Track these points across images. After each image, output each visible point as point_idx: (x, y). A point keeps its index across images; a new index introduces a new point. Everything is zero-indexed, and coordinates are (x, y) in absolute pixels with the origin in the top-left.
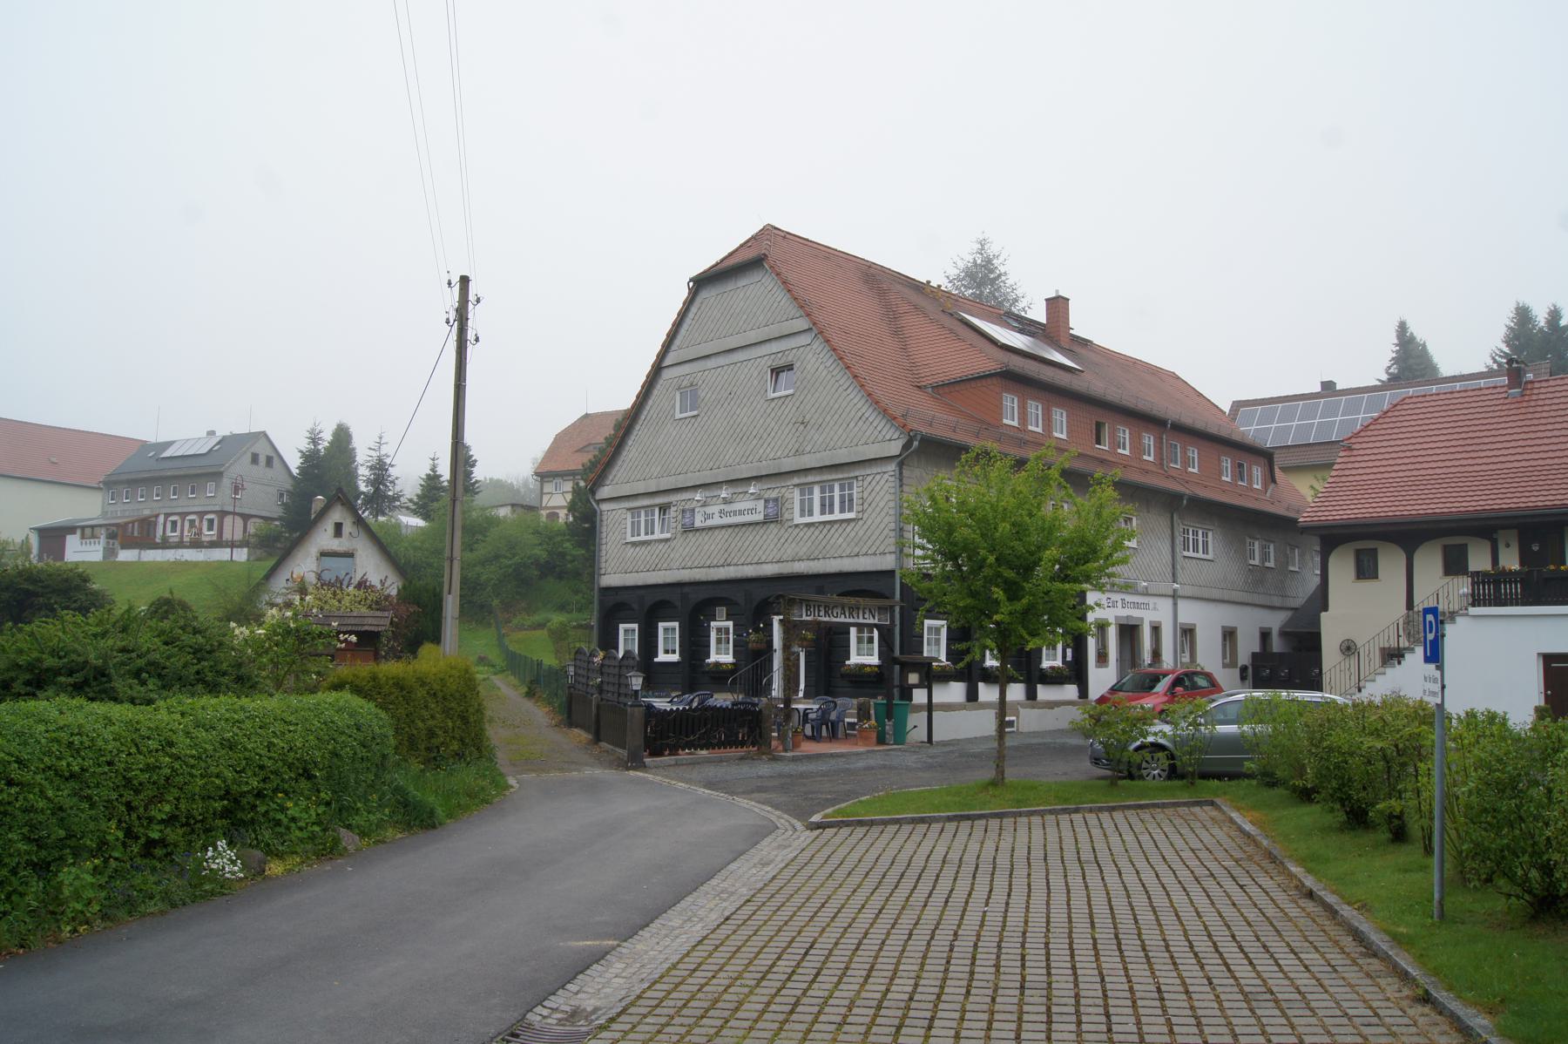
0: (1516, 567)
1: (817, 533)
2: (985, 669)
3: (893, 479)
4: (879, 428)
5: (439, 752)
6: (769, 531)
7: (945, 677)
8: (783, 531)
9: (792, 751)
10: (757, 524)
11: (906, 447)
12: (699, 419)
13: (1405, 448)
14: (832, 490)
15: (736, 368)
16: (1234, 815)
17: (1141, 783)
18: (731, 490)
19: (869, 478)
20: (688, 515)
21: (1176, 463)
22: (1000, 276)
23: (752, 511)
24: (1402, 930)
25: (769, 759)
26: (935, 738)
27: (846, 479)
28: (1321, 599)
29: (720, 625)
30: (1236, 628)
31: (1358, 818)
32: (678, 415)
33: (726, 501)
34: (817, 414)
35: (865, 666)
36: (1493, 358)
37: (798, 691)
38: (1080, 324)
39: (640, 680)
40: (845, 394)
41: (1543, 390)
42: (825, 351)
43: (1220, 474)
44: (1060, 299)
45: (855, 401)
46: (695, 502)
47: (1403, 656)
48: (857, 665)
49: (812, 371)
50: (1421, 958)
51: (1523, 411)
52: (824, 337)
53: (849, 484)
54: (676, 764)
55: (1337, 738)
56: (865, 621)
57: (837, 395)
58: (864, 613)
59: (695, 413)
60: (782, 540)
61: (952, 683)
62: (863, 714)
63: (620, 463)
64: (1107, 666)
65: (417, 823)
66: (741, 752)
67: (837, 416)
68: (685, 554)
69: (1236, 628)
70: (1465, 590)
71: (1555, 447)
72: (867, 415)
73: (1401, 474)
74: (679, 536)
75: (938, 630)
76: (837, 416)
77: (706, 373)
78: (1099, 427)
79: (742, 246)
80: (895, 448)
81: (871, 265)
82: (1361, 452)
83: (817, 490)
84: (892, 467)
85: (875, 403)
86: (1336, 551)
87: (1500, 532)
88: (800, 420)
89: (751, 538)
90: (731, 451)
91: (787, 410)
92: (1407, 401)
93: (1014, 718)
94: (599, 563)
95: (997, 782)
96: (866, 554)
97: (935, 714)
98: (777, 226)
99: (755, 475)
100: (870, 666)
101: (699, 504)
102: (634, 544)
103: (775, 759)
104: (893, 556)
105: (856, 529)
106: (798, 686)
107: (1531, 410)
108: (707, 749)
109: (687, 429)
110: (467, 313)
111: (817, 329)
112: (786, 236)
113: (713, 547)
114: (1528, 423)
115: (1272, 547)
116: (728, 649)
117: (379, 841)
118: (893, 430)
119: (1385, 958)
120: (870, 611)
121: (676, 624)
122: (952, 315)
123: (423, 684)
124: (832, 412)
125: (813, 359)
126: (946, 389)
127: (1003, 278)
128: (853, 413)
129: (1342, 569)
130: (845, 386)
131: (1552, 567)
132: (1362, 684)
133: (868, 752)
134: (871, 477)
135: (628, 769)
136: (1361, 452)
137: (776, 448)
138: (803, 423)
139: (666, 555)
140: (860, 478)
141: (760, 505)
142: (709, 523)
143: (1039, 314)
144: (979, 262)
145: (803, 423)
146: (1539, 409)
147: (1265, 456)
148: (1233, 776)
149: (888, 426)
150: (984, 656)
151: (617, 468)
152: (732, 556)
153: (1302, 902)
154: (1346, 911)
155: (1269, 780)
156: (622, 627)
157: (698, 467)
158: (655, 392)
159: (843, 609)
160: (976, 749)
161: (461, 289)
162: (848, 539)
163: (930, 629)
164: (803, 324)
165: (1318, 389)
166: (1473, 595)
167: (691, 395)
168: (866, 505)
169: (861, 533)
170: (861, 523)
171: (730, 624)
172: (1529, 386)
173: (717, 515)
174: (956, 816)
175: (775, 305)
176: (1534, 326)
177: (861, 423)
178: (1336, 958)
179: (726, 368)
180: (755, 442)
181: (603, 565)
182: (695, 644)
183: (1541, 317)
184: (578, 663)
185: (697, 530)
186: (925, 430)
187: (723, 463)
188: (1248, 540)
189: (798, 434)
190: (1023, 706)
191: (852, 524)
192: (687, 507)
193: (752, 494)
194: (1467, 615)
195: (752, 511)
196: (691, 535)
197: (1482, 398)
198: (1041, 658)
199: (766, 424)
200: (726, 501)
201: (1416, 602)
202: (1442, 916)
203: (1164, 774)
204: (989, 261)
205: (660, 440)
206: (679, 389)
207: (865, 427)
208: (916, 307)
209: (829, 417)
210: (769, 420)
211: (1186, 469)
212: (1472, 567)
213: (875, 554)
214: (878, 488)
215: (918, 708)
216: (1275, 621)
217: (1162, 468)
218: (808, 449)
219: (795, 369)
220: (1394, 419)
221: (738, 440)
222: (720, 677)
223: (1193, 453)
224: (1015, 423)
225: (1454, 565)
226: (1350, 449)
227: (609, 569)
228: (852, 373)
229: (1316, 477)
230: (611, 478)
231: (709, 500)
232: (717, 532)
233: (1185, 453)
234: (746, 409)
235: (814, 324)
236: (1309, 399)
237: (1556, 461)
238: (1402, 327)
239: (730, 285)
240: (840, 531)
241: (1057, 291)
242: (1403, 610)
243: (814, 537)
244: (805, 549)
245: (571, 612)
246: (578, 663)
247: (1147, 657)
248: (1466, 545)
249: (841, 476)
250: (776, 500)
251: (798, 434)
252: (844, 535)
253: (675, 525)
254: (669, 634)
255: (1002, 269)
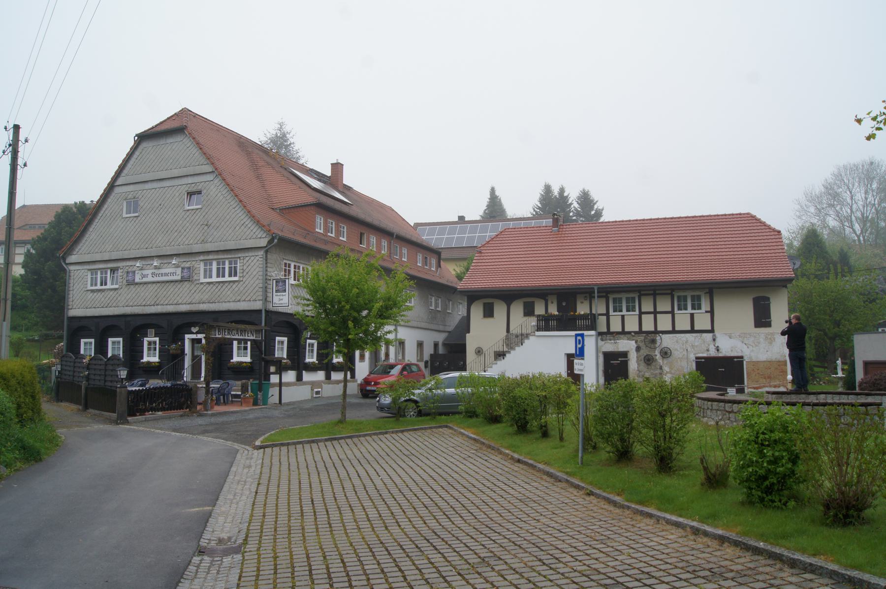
0: (556, 313)
1: (215, 287)
2: (306, 364)
3: (262, 259)
4: (254, 231)
5: (22, 417)
6: (184, 286)
7: (287, 368)
8: (193, 286)
9: (210, 410)
10: (176, 281)
11: (270, 242)
12: (139, 218)
13: (513, 253)
14: (224, 264)
15: (164, 191)
16: (462, 431)
17: (405, 418)
18: (160, 261)
19: (247, 258)
20: (131, 275)
21: (397, 256)
22: (290, 144)
23: (173, 274)
24: (568, 470)
25: (198, 416)
26: (283, 401)
27: (221, 259)
28: (465, 326)
29: (150, 339)
30: (423, 342)
31: (522, 427)
32: (125, 215)
33: (156, 268)
34: (216, 221)
35: (243, 363)
36: (534, 209)
37: (200, 377)
38: (347, 180)
39: (126, 372)
40: (233, 210)
41: (567, 230)
42: (223, 184)
43: (417, 262)
44: (339, 165)
45: (240, 215)
46: (135, 267)
47: (505, 355)
48: (238, 362)
49: (214, 196)
50: (582, 479)
51: (559, 239)
52: (222, 177)
53: (234, 261)
54: (145, 420)
55: (517, 392)
56: (249, 338)
57: (229, 210)
58: (248, 333)
59: (136, 214)
60: (193, 291)
61: (319, 372)
62: (244, 389)
63: (83, 241)
64: (364, 362)
65: (32, 458)
66: (181, 412)
67: (228, 223)
68: (128, 297)
69: (423, 342)
70: (534, 323)
71: (516, 244)
72: (247, 223)
73: (505, 266)
74: (124, 287)
75: (282, 342)
76: (228, 223)
77: (145, 191)
78: (362, 234)
79: (168, 118)
80: (264, 242)
81: (241, 137)
82: (486, 254)
83: (215, 264)
84: (261, 253)
85: (252, 217)
86: (516, 301)
87: (549, 296)
88: (205, 223)
89: (172, 289)
90: (160, 238)
91: (197, 217)
92: (507, 230)
93: (320, 390)
94: (68, 302)
95: (342, 421)
96: (244, 301)
97: (283, 388)
98: (190, 109)
99: (175, 253)
100: (245, 362)
101: (138, 269)
102: (92, 291)
103: (201, 415)
104: (261, 302)
105: (239, 286)
106: (201, 374)
107: (562, 238)
108: (161, 411)
109: (131, 225)
110: (18, 148)
111: (217, 172)
112: (195, 116)
113: (147, 294)
114: (561, 244)
115: (440, 300)
116: (156, 353)
117: (17, 470)
118: (262, 232)
119: (567, 481)
120: (251, 333)
121: (121, 339)
122: (286, 169)
123: (14, 376)
124: (226, 220)
125: (214, 189)
126: (286, 211)
127: (292, 145)
128: (238, 221)
129: (477, 312)
130: (234, 206)
131: (572, 313)
132: (486, 369)
133: (251, 410)
134: (248, 258)
135: (118, 424)
136: (486, 254)
137: (190, 238)
138: (207, 225)
139: (115, 299)
140: (242, 258)
141: (179, 271)
142: (145, 280)
143: (328, 172)
144: (279, 135)
145: (207, 225)
146: (566, 238)
147: (436, 253)
148: (454, 413)
149: (260, 230)
150: (333, 357)
151: (81, 245)
152: (160, 299)
153: (516, 464)
154: (541, 466)
155: (471, 414)
156: (83, 341)
157: (138, 247)
158: (109, 200)
159: (237, 331)
160: (307, 406)
161: (14, 133)
162: (234, 292)
163: (279, 342)
164: (209, 168)
165: (456, 219)
166: (537, 326)
167: (134, 205)
168: (245, 274)
169: (242, 288)
170: (242, 283)
171: (157, 339)
172: (562, 227)
173: (150, 276)
174: (329, 439)
175: (191, 155)
176: (552, 195)
177: (243, 227)
178: (546, 484)
179: (158, 189)
180: (176, 234)
181: (70, 303)
182: (133, 350)
183: (556, 191)
184: (64, 363)
185: (137, 284)
186: (281, 234)
187: (155, 245)
188: (430, 297)
189: (203, 231)
190: (325, 383)
191: (236, 284)
192: (130, 270)
193: (174, 264)
194: (534, 335)
195: (173, 274)
196: (132, 286)
197: (534, 232)
198: (305, 357)
199: (183, 224)
200: (156, 268)
201: (511, 329)
202: (582, 464)
203: (415, 414)
204: (284, 135)
205: (112, 230)
206: (126, 199)
207: (246, 229)
208: (268, 164)
209: (223, 223)
210: (185, 222)
211: (401, 258)
212: (537, 312)
213: (250, 301)
214: (252, 264)
215: (274, 385)
216: (440, 338)
217: (391, 258)
218: (210, 240)
219: (203, 194)
220: (501, 239)
221: (165, 232)
222: (151, 370)
223: (405, 251)
224: (322, 231)
225: (529, 311)
226: (480, 252)
227: (75, 307)
228: (238, 199)
229: (456, 265)
230: (77, 250)
231: (145, 266)
232: (150, 285)
233: (401, 251)
234: (170, 215)
235: (216, 169)
236: (452, 224)
237: (573, 264)
238: (493, 191)
239: (162, 141)
240: (229, 287)
241: (337, 160)
242: (505, 334)
243: (212, 290)
244: (207, 297)
245: (20, 331)
246: (64, 363)
247: (383, 357)
248: (493, 303)
249: (230, 257)
250: (189, 268)
251: (203, 231)
252: (231, 289)
253: (121, 280)
254: (115, 346)
255: (292, 140)
